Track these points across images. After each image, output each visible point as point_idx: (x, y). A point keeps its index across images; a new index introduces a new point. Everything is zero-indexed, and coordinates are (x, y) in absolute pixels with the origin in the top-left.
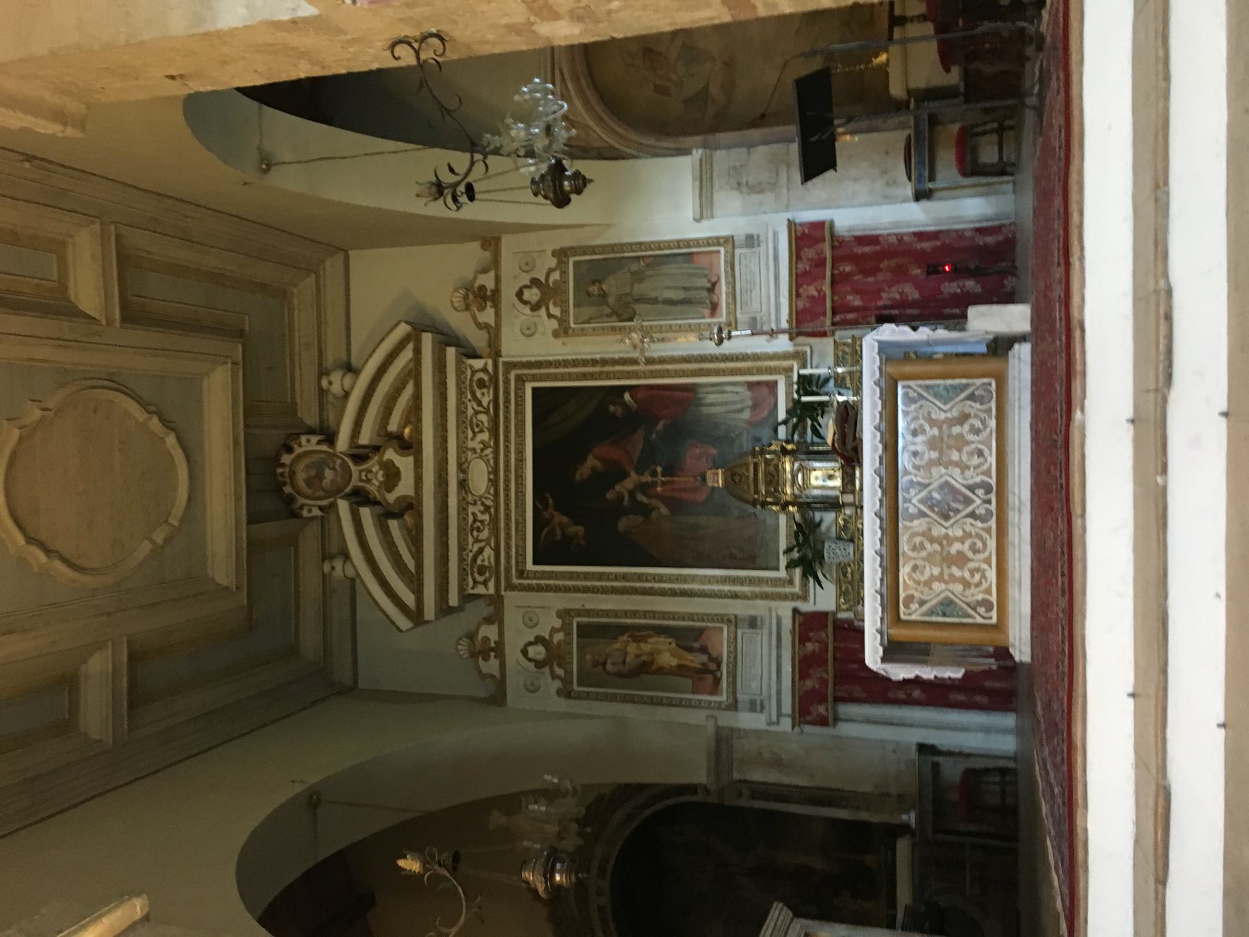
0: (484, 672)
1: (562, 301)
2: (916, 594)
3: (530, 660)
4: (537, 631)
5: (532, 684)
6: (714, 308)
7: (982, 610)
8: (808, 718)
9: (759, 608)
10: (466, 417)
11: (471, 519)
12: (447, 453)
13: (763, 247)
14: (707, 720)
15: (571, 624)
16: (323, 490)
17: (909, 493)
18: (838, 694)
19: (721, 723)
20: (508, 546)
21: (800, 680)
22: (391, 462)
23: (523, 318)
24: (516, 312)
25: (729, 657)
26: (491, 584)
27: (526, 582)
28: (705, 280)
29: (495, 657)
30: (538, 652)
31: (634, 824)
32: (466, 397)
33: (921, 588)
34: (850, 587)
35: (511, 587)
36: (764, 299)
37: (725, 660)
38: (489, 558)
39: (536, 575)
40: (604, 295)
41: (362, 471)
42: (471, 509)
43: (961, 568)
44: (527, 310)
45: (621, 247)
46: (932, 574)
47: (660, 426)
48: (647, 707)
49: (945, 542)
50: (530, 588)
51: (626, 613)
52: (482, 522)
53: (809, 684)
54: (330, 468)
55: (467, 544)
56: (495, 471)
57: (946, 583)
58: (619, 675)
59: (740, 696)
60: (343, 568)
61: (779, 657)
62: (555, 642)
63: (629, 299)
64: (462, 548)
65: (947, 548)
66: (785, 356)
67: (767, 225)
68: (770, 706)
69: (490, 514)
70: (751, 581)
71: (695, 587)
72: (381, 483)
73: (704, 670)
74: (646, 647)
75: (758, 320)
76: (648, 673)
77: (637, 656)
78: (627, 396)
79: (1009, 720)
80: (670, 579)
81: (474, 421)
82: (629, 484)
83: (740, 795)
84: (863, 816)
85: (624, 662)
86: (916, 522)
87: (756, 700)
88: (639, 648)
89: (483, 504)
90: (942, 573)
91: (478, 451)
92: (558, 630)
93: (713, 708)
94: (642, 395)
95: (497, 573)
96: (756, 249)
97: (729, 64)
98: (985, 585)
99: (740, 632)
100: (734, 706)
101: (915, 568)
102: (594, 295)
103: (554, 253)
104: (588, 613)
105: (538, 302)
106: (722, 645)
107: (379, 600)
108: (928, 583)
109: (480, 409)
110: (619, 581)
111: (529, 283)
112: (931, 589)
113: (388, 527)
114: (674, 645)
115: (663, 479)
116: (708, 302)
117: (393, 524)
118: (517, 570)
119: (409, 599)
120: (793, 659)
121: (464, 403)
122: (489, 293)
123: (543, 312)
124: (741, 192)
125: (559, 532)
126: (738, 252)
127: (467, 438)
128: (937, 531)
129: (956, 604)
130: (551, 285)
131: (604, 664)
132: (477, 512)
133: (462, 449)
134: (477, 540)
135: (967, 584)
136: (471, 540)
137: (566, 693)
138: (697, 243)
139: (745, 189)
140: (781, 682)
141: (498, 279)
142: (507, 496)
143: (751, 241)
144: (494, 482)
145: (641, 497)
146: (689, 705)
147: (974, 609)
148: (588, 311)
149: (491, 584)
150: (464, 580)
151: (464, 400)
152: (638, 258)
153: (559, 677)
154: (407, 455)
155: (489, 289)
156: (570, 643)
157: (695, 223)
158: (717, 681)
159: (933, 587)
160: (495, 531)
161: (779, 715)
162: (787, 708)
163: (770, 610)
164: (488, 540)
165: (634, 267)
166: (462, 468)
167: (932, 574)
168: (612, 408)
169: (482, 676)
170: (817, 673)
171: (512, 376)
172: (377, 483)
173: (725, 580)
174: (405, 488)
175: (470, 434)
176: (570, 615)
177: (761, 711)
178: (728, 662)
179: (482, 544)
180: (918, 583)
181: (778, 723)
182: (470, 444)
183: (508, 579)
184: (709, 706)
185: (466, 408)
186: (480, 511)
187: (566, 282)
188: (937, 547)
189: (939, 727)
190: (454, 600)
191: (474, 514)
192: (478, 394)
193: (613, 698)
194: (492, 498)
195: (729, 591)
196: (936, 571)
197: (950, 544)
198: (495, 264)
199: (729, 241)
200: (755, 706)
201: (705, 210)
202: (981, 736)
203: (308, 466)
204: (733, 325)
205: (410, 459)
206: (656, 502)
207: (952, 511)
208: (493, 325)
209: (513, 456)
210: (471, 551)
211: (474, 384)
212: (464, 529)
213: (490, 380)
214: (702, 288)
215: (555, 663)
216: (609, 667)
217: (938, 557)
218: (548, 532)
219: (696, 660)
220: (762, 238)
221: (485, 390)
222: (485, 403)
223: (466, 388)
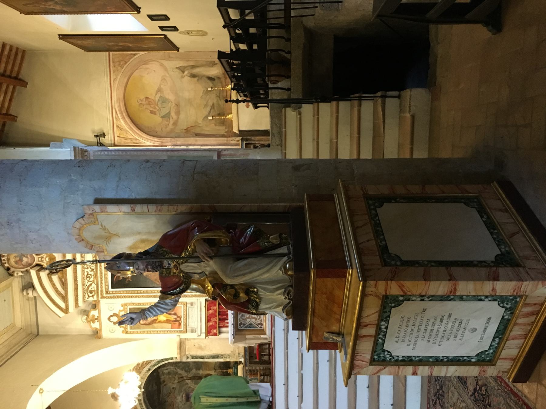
2: (243, 322)
7: (260, 326)
8: (210, 334)
11: (86, 274)
16: (23, 265)
18: (220, 326)
19: (181, 338)
20: (101, 283)
26: (95, 297)
27: (109, 295)
31: (151, 372)
33: (244, 321)
35: (103, 297)
38: (94, 288)
50: (111, 297)
52: (91, 275)
53: (211, 323)
54: (25, 257)
57: (251, 319)
59: (188, 329)
69: (94, 272)
73: (176, 321)
76: (155, 323)
83: (188, 358)
84: (228, 360)
89: (91, 268)
90: (249, 316)
92: (122, 311)
97: (177, 105)
98: (260, 319)
106: (181, 312)
107: (46, 302)
118: (105, 291)
119: (63, 305)
129: (253, 325)
132: (88, 271)
134: (89, 281)
135: (256, 319)
147: (258, 326)
149: (95, 297)
150: (84, 296)
158: (180, 324)
161: (201, 333)
162: (204, 330)
170: (213, 319)
172: (46, 262)
179: (91, 283)
180: (243, 319)
181: (200, 335)
191: (87, 272)
200: (193, 331)
203: (16, 257)
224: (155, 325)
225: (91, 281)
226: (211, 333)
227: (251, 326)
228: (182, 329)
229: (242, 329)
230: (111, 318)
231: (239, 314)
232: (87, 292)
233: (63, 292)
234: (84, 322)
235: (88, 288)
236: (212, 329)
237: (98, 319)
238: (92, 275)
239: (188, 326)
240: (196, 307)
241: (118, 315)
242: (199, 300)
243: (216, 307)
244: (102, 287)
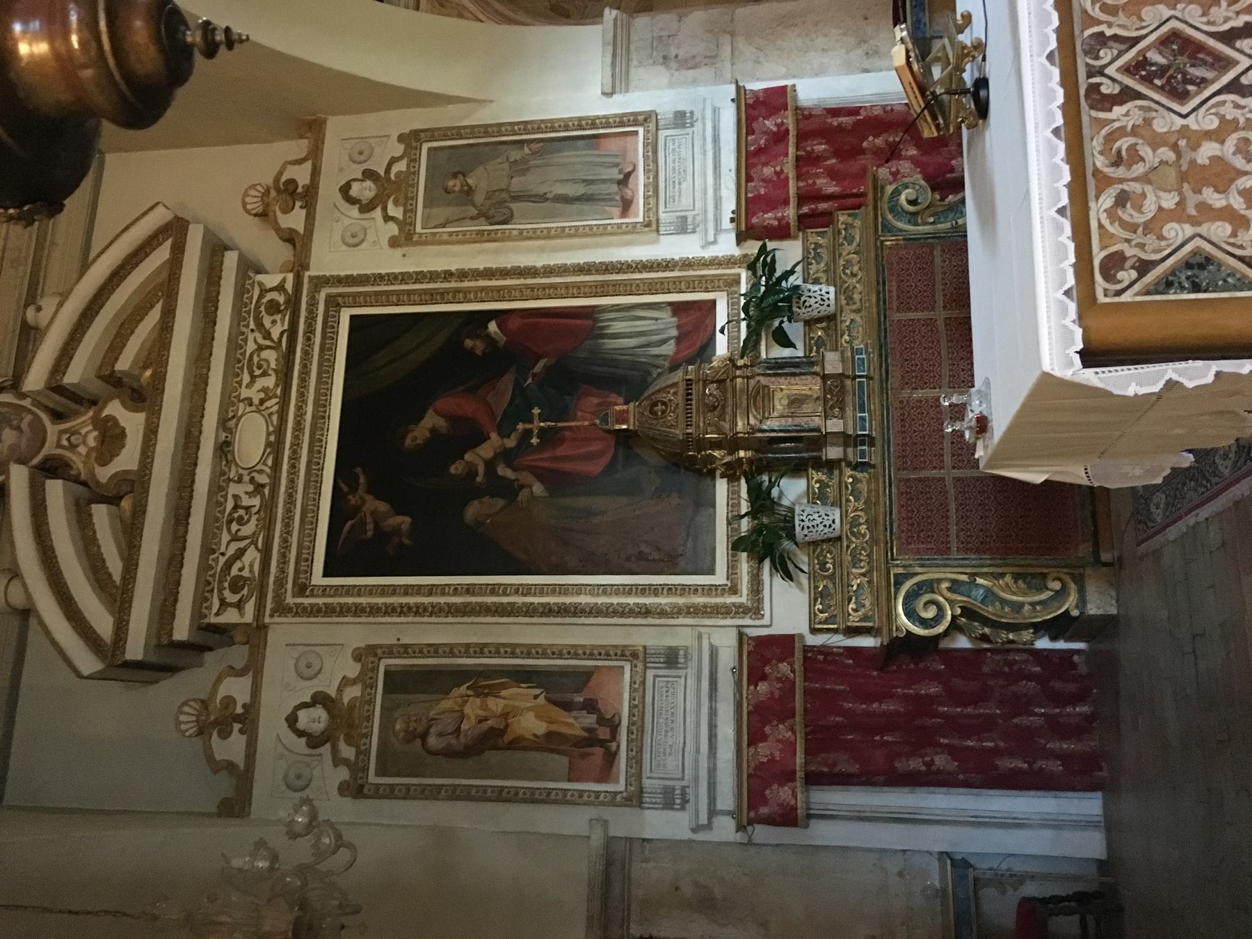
0: (218, 757)
1: (406, 198)
2: (1129, 252)
3: (300, 734)
4: (318, 685)
5: (299, 777)
6: (626, 206)
9: (680, 635)
10: (243, 354)
11: (230, 504)
12: (205, 401)
13: (698, 127)
14: (591, 827)
15: (375, 669)
17: (1097, 58)
19: (613, 832)
20: (285, 543)
21: (749, 745)
22: (112, 419)
23: (347, 221)
24: (337, 214)
25: (631, 715)
26: (250, 607)
27: (306, 601)
28: (616, 170)
29: (241, 731)
30: (314, 719)
32: (247, 326)
33: (1138, 238)
34: (830, 586)
35: (282, 609)
36: (698, 194)
37: (625, 722)
38: (251, 566)
39: (325, 591)
40: (469, 191)
41: (65, 431)
42: (233, 489)
43: (1222, 190)
44: (354, 211)
45: (499, 128)
46: (1160, 209)
47: (539, 367)
48: (489, 806)
49: (1182, 143)
51: (467, 649)
52: (247, 508)
54: (11, 427)
55: (219, 543)
56: (280, 430)
57: (1195, 222)
58: (449, 753)
59: (647, 783)
60: (6, 587)
61: (713, 713)
62: (346, 701)
63: (505, 195)
64: (208, 549)
65: (1187, 156)
66: (729, 262)
67: (705, 100)
68: (697, 796)
69: (263, 497)
70: (671, 590)
71: (583, 599)
72: (91, 450)
73: (591, 740)
74: (496, 705)
75: (690, 220)
77: (481, 720)
78: (493, 327)
79: (1090, 805)
80: (541, 590)
81: (256, 359)
82: (486, 451)
85: (458, 730)
86: (1118, 111)
87: (674, 789)
88: (484, 707)
89: (252, 480)
90: (1181, 204)
91: (256, 401)
92: (354, 682)
93: (603, 804)
94: (514, 324)
95: (262, 587)
96: (689, 131)
99: (650, 674)
100: (636, 799)
101: (1122, 200)
102: (454, 192)
103: (401, 138)
104: (405, 650)
105: (372, 201)
108: (1152, 227)
109: (268, 343)
110: (461, 595)
111: (360, 176)
112: (1161, 237)
113: (91, 515)
114: (541, 700)
115: (542, 424)
116: (618, 198)
117: (100, 513)
119: (103, 623)
120: (738, 706)
121: (243, 333)
122: (300, 190)
123: (378, 213)
124: (667, 67)
125: (370, 527)
126: (662, 134)
127: (240, 383)
128: (1164, 123)
130: (393, 177)
131: (424, 736)
133: (229, 400)
134: (235, 538)
136: (225, 537)
137: (355, 789)
138: (606, 121)
139: (673, 64)
140: (715, 757)
141: (316, 172)
142: (293, 467)
143: (682, 119)
144: (275, 447)
145: (503, 471)
146: (564, 800)
148: (442, 213)
149: (250, 607)
151: (244, 330)
152: (522, 142)
153: (346, 762)
154: (135, 410)
155: (300, 185)
156: (371, 702)
157: (604, 98)
158: (611, 757)
159: (1165, 232)
160: (267, 525)
161: (713, 813)
162: (726, 799)
163: (700, 637)
164: (253, 539)
165: (515, 155)
166: (226, 422)
167: (1160, 209)
168: (468, 343)
169: (215, 766)
171: (322, 297)
173: (629, 590)
174: (127, 459)
175: (246, 378)
176: (376, 655)
177: (683, 808)
178: (631, 723)
179: (242, 544)
180: (1133, 228)
181: (709, 826)
182: (245, 393)
183: (279, 597)
184: (596, 800)
185: (246, 340)
186: (246, 493)
187: (416, 173)
188: (1166, 154)
189: (978, 822)
190: (181, 631)
191: (236, 497)
192: (267, 321)
193: (433, 794)
194: (268, 470)
195: (637, 604)
196: (1169, 201)
197: (1195, 147)
198: (315, 154)
199: (645, 118)
200: (672, 799)
201: (617, 83)
202: (1047, 834)
204: (654, 226)
205: (141, 417)
206: (526, 477)
207: (1192, 82)
208: (301, 231)
209: (310, 409)
210: (223, 554)
211: (262, 308)
212: (217, 520)
213: (287, 302)
214: (611, 181)
215: (342, 737)
216: (432, 741)
217: (1172, 175)
218: (353, 526)
219: (576, 723)
220: (697, 115)
221: (278, 317)
222: (275, 335)
223: (249, 312)
224: (493, 757)
225: (245, 538)
226: (766, 803)
227: (1203, 276)
228: (621, 786)
229: (1126, 298)
230: (302, 714)
231: (1092, 192)
232: (221, 582)
233: (115, 566)
234: (183, 732)
235: (228, 565)
236: (769, 786)
237: (248, 719)
238: (255, 510)
239: (646, 772)
240: (691, 672)
241: (332, 700)
242: (705, 637)
243: (791, 664)
244: (284, 557)
